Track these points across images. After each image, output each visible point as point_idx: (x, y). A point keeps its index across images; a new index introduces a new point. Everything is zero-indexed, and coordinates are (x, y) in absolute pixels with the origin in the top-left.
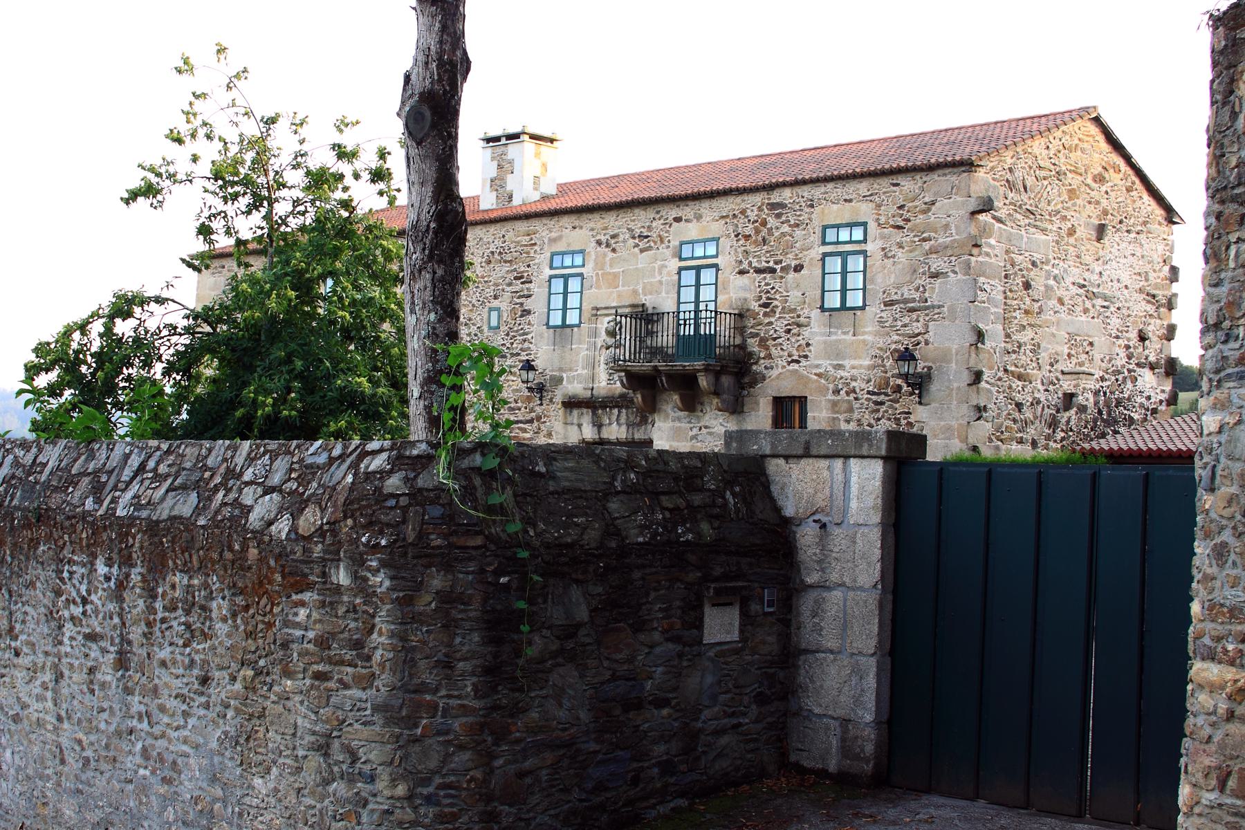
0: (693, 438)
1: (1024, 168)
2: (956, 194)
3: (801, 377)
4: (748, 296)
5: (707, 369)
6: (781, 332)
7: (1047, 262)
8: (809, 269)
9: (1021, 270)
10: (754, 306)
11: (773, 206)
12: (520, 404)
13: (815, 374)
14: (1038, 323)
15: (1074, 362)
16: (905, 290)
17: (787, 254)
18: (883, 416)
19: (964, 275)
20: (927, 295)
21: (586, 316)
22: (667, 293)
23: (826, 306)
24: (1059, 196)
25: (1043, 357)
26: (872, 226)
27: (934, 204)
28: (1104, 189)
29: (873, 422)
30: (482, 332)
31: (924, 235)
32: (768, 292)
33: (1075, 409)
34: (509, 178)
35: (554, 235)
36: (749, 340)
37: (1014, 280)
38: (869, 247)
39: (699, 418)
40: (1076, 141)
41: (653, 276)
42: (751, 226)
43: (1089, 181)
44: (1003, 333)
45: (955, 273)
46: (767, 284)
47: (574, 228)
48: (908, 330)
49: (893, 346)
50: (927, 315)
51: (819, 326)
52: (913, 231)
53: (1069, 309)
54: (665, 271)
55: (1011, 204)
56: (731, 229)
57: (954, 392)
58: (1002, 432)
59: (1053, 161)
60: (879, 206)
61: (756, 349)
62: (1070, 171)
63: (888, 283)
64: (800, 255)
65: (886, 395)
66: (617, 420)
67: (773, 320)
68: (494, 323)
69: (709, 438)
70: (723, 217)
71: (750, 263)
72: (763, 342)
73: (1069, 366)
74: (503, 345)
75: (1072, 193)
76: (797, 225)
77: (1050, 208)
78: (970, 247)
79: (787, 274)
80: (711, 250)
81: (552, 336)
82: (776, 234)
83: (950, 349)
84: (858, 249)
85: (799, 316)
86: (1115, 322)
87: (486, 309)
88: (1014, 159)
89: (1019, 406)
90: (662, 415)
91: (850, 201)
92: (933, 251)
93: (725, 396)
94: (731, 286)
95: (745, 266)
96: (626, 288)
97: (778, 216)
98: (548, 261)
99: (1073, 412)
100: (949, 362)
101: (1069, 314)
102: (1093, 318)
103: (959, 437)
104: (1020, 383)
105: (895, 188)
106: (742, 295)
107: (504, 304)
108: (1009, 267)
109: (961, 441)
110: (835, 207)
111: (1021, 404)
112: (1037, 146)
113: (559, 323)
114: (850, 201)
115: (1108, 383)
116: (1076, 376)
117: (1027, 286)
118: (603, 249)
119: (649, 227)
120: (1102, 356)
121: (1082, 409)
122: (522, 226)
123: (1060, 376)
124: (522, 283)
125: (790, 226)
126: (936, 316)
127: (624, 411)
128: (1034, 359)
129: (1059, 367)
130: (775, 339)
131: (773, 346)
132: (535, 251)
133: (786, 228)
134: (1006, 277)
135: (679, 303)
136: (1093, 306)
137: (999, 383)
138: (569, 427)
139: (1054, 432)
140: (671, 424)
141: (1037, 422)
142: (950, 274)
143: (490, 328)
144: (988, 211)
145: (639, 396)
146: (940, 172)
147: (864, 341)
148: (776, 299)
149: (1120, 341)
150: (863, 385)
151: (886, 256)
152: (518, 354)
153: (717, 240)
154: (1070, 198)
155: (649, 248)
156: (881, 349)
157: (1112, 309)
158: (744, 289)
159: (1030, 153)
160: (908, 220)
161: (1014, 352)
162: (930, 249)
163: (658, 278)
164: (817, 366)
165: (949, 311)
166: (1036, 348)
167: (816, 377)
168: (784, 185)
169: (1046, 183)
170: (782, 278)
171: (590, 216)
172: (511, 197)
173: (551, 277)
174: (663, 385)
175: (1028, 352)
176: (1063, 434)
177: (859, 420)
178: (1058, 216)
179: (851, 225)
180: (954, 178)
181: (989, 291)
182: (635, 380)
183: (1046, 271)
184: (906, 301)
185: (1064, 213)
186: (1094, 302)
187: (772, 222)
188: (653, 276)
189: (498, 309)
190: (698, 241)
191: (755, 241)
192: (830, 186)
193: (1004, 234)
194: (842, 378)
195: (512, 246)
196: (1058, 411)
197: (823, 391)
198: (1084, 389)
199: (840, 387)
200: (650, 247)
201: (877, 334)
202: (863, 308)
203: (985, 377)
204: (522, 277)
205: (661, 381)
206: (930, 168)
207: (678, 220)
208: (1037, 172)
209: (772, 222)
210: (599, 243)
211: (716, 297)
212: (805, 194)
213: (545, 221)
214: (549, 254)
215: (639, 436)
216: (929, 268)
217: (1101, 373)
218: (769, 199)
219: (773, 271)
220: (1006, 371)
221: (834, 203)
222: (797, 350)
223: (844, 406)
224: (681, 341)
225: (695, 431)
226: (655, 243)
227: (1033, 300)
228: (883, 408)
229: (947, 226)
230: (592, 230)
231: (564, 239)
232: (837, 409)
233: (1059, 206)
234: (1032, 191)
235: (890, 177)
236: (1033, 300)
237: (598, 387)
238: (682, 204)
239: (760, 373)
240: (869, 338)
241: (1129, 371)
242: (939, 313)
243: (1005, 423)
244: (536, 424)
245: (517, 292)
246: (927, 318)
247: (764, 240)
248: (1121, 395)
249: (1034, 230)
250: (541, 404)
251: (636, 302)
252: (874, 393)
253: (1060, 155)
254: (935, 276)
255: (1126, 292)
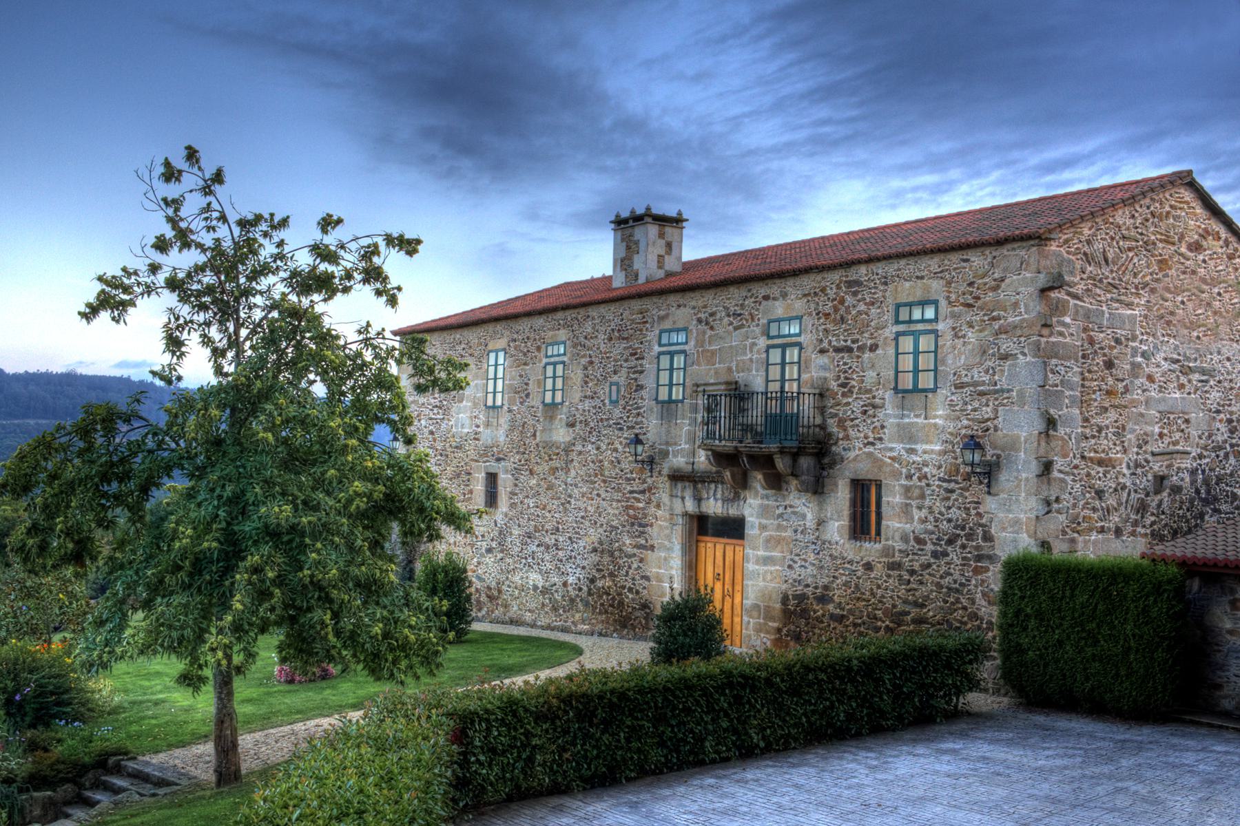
0: (780, 516)
1: (1104, 239)
2: (1025, 270)
3: (876, 460)
4: (828, 375)
5: (782, 451)
6: (858, 411)
7: (1134, 338)
8: (883, 349)
9: (1102, 348)
10: (833, 385)
11: (850, 284)
12: (634, 475)
13: (890, 458)
14: (1123, 403)
15: (1166, 442)
16: (975, 371)
17: (863, 333)
18: (953, 505)
19: (1033, 357)
20: (996, 377)
21: (688, 391)
22: (757, 371)
23: (900, 387)
24: (1148, 267)
25: (1130, 440)
26: (943, 303)
27: (1003, 281)
28: (1201, 257)
29: (943, 510)
30: (604, 405)
31: (994, 314)
32: (846, 372)
33: (1168, 491)
34: (636, 257)
35: (662, 313)
36: (829, 420)
37: (1093, 359)
38: (940, 326)
39: (784, 497)
40: (1167, 208)
41: (745, 354)
42: (830, 304)
43: (1183, 250)
44: (1080, 418)
45: (1024, 354)
46: (845, 364)
47: (679, 306)
48: (977, 415)
49: (963, 432)
50: (996, 399)
51: (893, 408)
52: (982, 310)
53: (1160, 387)
54: (755, 350)
55: (1089, 278)
56: (813, 306)
57: (1023, 483)
58: (1079, 523)
59: (1140, 231)
60: (949, 283)
61: (835, 430)
62: (1161, 241)
63: (959, 364)
64: (876, 334)
65: (957, 483)
66: (714, 495)
67: (850, 400)
68: (614, 397)
69: (793, 518)
70: (805, 295)
71: (830, 342)
72: (841, 423)
73: (1160, 446)
74: (621, 418)
75: (1163, 264)
76: (873, 304)
77: (1136, 281)
78: (1039, 327)
79: (863, 353)
80: (795, 329)
82: (854, 312)
83: (1019, 437)
84: (930, 328)
85: (874, 397)
86: (1215, 395)
87: (608, 384)
88: (1093, 230)
89: (1100, 494)
90: (753, 492)
91: (922, 278)
92: (1002, 331)
93: (804, 478)
94: (813, 365)
95: (825, 345)
97: (855, 294)
98: (656, 339)
99: (1165, 494)
100: (1018, 450)
101: (1160, 391)
102: (1189, 393)
103: (1027, 532)
104: (1101, 469)
105: (965, 264)
106: (823, 374)
107: (621, 378)
108: (1086, 345)
109: (1030, 536)
110: (907, 284)
111: (1103, 491)
112: (1121, 217)
113: (666, 398)
114: (922, 278)
115: (1207, 460)
116: (1169, 457)
117: (1109, 365)
118: (702, 327)
119: (742, 305)
120: (1200, 432)
121: (1176, 490)
122: (636, 305)
123: (1150, 458)
124: (637, 359)
125: (866, 304)
126: (1005, 401)
127: (720, 486)
128: (1118, 442)
129: (1149, 448)
130: (852, 420)
131: (852, 426)
132: (647, 329)
133: (862, 307)
134: (1084, 357)
135: (767, 381)
136: (1190, 381)
137: (1075, 471)
138: (674, 499)
139: (1142, 517)
140: (760, 502)
141: (1123, 508)
142: (1020, 356)
143: (611, 402)
144: (1061, 287)
145: (728, 473)
146: (1009, 246)
147: (935, 425)
148: (853, 379)
149: (1222, 416)
150: (935, 472)
151: (956, 336)
152: (633, 427)
153: (800, 318)
154: (1161, 269)
155: (742, 326)
156: (951, 434)
157: (1212, 383)
158: (824, 368)
159: (1112, 223)
160: (977, 298)
161: (1093, 437)
162: (1000, 329)
163: (749, 356)
164: (891, 449)
165: (1017, 395)
166: (1120, 431)
167: (889, 461)
168: (859, 262)
169: (1131, 254)
170: (858, 357)
171: (692, 295)
172: (637, 276)
173: (660, 354)
175: (1110, 435)
176: (1153, 518)
177: (930, 508)
178: (1147, 289)
179: (923, 303)
180: (1023, 253)
181: (1063, 373)
182: (724, 459)
183: (1133, 348)
184: (975, 384)
185: (1154, 285)
186: (1191, 377)
187: (849, 300)
188: (745, 354)
189: (617, 384)
190: (784, 320)
191: (835, 320)
192: (903, 262)
193: (1081, 311)
194: (914, 463)
195: (628, 323)
196: (1147, 495)
197: (896, 475)
198: (1179, 468)
199: (913, 471)
200: (743, 325)
201: (947, 418)
202: (934, 391)
203: (1056, 467)
204: (636, 354)
206: (1000, 243)
207: (766, 298)
208: (1121, 243)
209: (849, 300)
210: (700, 321)
211: (799, 376)
212: (880, 271)
213: (655, 299)
214: (658, 332)
215: (733, 512)
216: (999, 350)
217: (1199, 451)
218: (847, 276)
219: (850, 350)
220: (1083, 457)
221: (906, 280)
222: (873, 432)
223: (917, 492)
225: (781, 510)
226: (747, 320)
227: (1117, 380)
228: (954, 496)
229: (1016, 305)
230: (694, 308)
231: (670, 317)
232: (909, 495)
233: (1148, 278)
234: (1114, 263)
235: (960, 252)
236: (1117, 380)
238: (770, 282)
239: (839, 454)
240: (939, 421)
241: (1232, 446)
242: (1008, 398)
243: (1082, 514)
244: (647, 495)
245: (632, 368)
246: (996, 403)
247: (842, 318)
248: (1223, 472)
249: (1116, 305)
250: (652, 476)
251: (730, 379)
252: (944, 481)
253: (1149, 224)
254: (1005, 357)
255: (1228, 364)
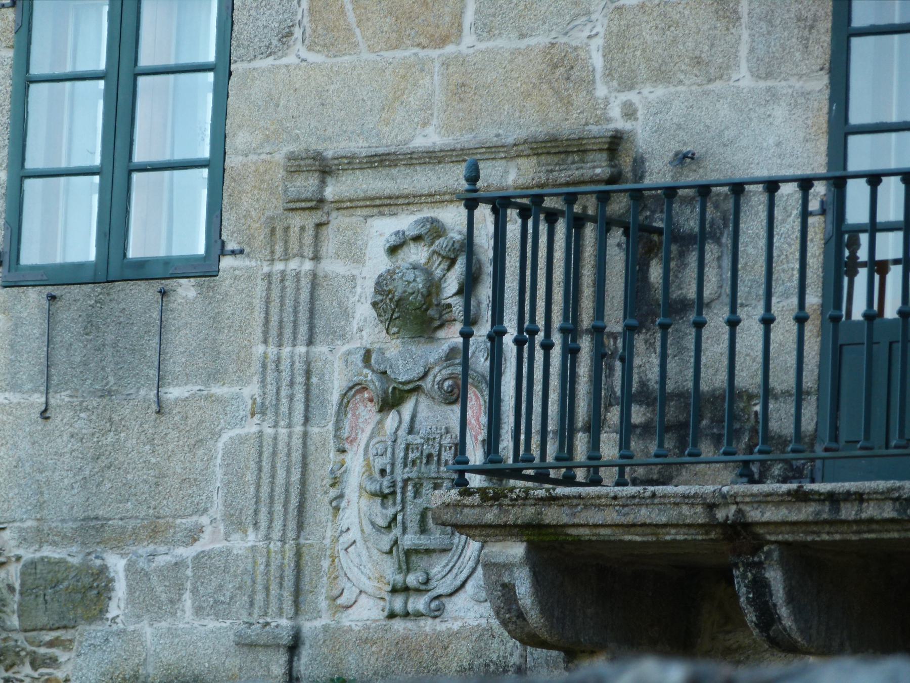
81: (36, 329)
96: (505, 43)
174: (767, 617)
205: (760, 587)
224: (855, 361)
237: (331, 634)
